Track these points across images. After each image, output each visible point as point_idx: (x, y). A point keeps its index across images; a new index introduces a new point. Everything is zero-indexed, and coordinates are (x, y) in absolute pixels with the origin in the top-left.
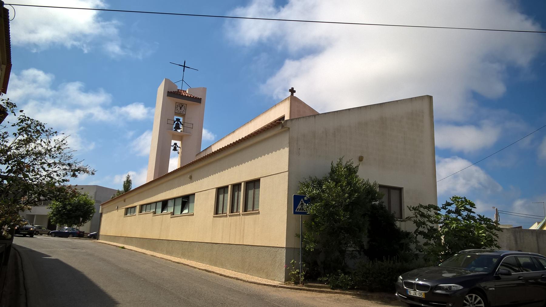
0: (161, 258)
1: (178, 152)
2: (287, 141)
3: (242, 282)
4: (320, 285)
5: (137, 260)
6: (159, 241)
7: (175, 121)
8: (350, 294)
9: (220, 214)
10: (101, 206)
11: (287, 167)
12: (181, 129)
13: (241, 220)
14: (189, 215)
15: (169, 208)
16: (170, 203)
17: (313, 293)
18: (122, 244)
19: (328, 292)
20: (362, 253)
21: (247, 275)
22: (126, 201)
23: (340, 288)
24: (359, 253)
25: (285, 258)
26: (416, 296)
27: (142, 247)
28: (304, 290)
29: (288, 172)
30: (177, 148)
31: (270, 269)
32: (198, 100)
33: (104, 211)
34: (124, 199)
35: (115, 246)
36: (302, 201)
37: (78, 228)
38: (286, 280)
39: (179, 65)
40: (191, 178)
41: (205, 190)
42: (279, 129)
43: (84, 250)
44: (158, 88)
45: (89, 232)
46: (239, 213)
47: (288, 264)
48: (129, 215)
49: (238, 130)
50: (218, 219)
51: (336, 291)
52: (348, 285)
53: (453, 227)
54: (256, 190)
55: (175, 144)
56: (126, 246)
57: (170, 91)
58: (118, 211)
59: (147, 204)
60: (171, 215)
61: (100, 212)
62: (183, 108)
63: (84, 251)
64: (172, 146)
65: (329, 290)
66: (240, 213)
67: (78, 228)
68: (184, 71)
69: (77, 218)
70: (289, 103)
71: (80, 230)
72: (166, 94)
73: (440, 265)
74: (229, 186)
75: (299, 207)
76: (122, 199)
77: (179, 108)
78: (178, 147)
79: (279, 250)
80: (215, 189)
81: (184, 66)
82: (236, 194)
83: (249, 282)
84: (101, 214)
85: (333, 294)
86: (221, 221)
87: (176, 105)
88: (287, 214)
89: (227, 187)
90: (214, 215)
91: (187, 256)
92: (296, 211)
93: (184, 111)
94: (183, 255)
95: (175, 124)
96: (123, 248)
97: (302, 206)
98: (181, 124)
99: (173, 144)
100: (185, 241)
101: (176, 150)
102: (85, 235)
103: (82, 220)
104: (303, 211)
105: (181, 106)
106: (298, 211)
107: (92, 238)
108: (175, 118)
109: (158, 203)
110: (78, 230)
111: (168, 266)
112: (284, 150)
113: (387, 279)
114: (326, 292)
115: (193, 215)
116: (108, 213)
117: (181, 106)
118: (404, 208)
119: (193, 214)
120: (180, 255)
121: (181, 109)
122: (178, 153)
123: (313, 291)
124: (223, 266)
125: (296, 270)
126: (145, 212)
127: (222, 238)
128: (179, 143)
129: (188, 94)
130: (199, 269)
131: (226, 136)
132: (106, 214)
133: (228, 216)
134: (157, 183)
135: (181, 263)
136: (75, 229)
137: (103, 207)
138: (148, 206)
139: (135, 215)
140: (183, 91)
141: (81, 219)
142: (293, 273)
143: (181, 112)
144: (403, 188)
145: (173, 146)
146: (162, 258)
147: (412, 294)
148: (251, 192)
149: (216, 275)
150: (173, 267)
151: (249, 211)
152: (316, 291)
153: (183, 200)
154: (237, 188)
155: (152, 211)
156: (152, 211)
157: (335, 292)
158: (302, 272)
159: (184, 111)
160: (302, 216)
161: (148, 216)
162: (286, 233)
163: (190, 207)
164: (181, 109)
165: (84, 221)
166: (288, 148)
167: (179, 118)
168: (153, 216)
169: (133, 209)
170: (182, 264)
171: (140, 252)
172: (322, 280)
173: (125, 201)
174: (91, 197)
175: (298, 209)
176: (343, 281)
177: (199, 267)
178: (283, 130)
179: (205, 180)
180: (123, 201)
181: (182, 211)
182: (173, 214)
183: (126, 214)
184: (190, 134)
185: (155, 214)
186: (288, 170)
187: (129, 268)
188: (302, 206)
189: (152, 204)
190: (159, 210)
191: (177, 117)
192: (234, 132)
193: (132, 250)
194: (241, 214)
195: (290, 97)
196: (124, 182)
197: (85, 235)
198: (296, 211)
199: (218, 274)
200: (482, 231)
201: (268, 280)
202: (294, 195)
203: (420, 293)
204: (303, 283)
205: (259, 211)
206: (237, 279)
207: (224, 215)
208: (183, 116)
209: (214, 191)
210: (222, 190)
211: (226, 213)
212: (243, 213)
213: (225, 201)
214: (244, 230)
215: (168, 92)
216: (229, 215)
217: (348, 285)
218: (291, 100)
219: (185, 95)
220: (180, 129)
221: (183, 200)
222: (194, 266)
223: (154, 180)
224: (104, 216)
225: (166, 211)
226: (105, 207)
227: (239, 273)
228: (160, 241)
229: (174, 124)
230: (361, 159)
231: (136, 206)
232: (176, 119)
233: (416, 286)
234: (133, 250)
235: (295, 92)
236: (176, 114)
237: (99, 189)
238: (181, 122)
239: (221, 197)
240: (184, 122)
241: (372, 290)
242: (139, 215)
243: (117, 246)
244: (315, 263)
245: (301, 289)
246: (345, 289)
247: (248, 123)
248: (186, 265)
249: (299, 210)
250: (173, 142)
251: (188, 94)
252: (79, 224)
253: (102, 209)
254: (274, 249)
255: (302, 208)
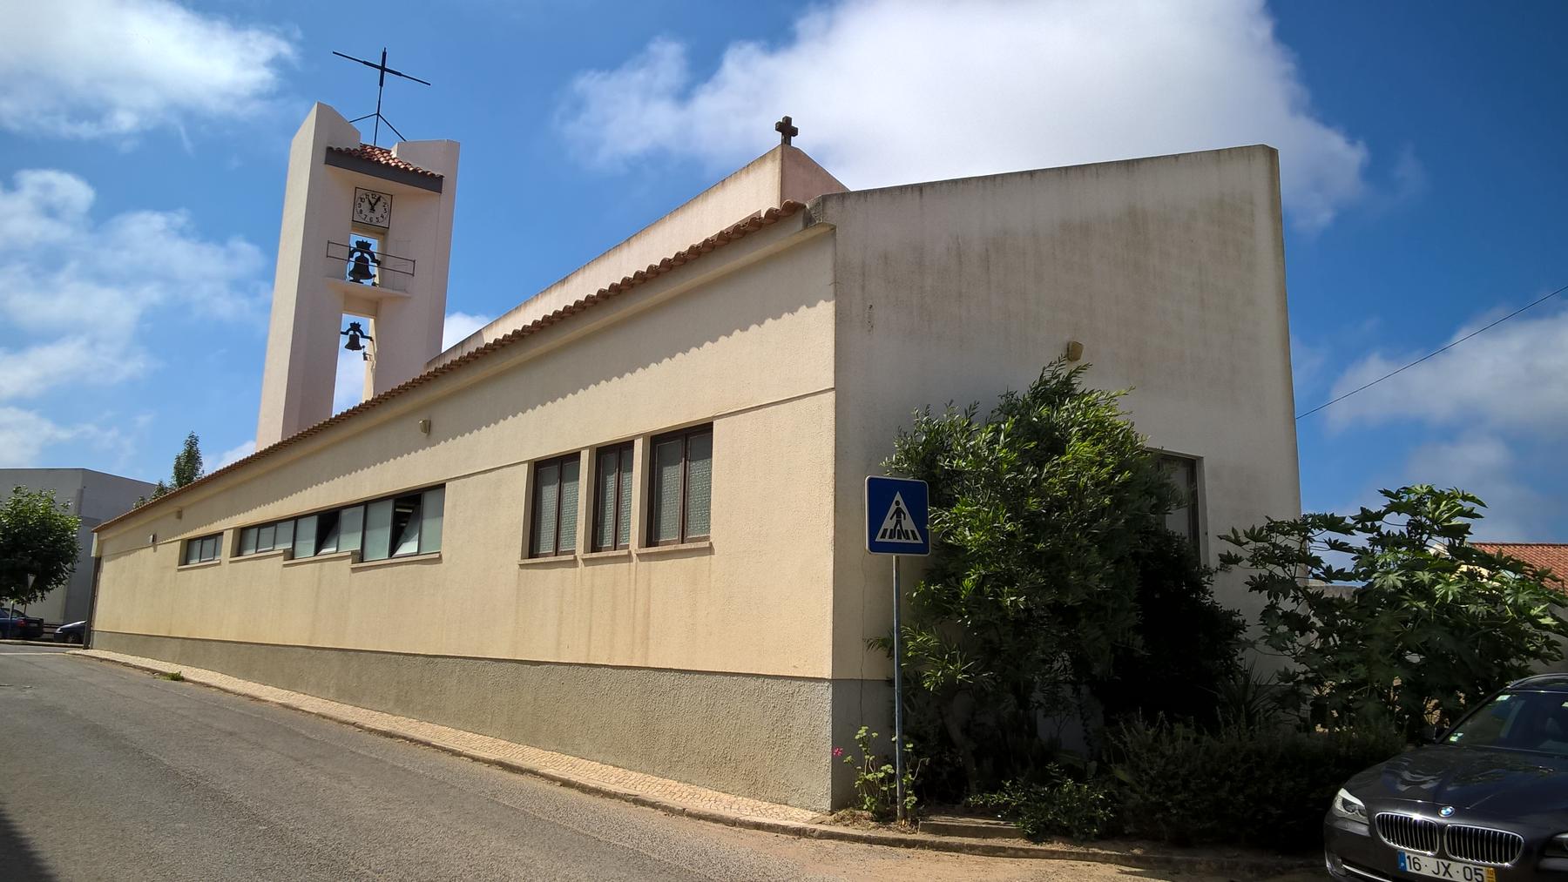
0: (319, 715)
1: (364, 354)
2: (828, 277)
3: (659, 812)
4: (980, 822)
5: (229, 728)
6: (309, 653)
7: (355, 250)
8: (1106, 860)
9: (546, 555)
10: (96, 534)
11: (831, 376)
12: (375, 276)
13: (633, 576)
14: (418, 559)
15: (344, 538)
16: (350, 520)
17: (962, 856)
18: (173, 661)
19: (1021, 853)
20: (1084, 689)
21: (667, 780)
22: (185, 514)
23: (1065, 834)
24: (1074, 690)
25: (828, 718)
26: (1447, 877)
27: (247, 674)
28: (922, 845)
29: (832, 395)
30: (362, 342)
31: (763, 761)
32: (432, 183)
33: (108, 550)
34: (177, 509)
35: (148, 669)
36: (898, 503)
37: (20, 608)
38: (837, 805)
39: (365, 63)
40: (427, 428)
41: (485, 472)
42: (793, 233)
43: (28, 692)
44: (295, 138)
45: (61, 622)
46: (625, 552)
47: (841, 739)
48: (194, 562)
49: (581, 272)
50: (541, 572)
51: (1047, 847)
52: (1092, 821)
53: (1453, 594)
54: (696, 467)
55: (355, 327)
56: (187, 672)
57: (335, 147)
58: (155, 551)
59: (261, 526)
60: (285, 560)
61: (93, 555)
62: (379, 208)
63: (28, 693)
64: (342, 333)
65: (1020, 843)
66: (630, 552)
67: (20, 608)
68: (381, 84)
69: (18, 575)
70: (777, 170)
71: (26, 614)
72: (323, 157)
73: (1453, 739)
74: (582, 452)
75: (888, 523)
76: (170, 509)
77: (366, 206)
78: (363, 337)
79: (802, 689)
80: (526, 465)
81: (383, 69)
82: (611, 481)
83: (690, 815)
84: (98, 562)
85: (1044, 861)
86: (551, 580)
87: (358, 196)
88: (832, 554)
89: (574, 456)
90: (523, 558)
91: (419, 707)
92: (878, 539)
93: (382, 216)
94: (404, 705)
95: (353, 259)
96: (177, 678)
97: (899, 522)
98: (374, 260)
99: (345, 327)
100: (411, 655)
101: (358, 348)
102: (46, 630)
103: (35, 581)
104: (903, 540)
105: (375, 200)
106: (887, 540)
107: (71, 639)
108: (354, 239)
109: (301, 523)
110: (23, 615)
111: (354, 750)
112: (812, 309)
113: (1241, 798)
114: (1012, 852)
115: (439, 560)
116: (122, 558)
117: (373, 201)
118: (1206, 527)
119: (437, 555)
120: (391, 704)
121: (372, 210)
122: (365, 359)
123: (958, 849)
124: (563, 745)
125: (883, 768)
126: (256, 552)
127: (559, 643)
128: (369, 325)
129: (396, 161)
130: (475, 759)
131: (537, 295)
132: (112, 563)
133: (580, 562)
134: (297, 452)
135: (399, 737)
136: (8, 610)
137: (102, 538)
138: (267, 533)
139: (219, 564)
140: (380, 150)
141: (31, 579)
142: (870, 777)
143: (375, 220)
144: (1201, 459)
145: (346, 333)
146: (324, 717)
147: (1426, 872)
148: (672, 475)
149: (542, 784)
150: (373, 756)
151: (668, 543)
152: (971, 849)
153: (397, 510)
154: (612, 458)
155: (280, 548)
156: (280, 548)
157: (1046, 851)
158: (903, 775)
159: (382, 216)
160: (897, 558)
161: (266, 569)
162: (829, 626)
163: (425, 531)
164: (372, 210)
165: (43, 584)
166: (833, 302)
167: (365, 240)
168: (285, 566)
169: (209, 544)
170: (405, 738)
171: (239, 694)
172: (986, 803)
173: (180, 515)
174: (65, 505)
175: (886, 530)
176: (1073, 808)
177: (472, 752)
178: (811, 233)
179: (509, 425)
180: (173, 518)
181: (394, 548)
182: (360, 556)
183: (185, 559)
184: (407, 295)
185: (293, 558)
186: (833, 387)
187: (200, 771)
188: (899, 522)
189: (279, 525)
190: (306, 547)
191: (360, 239)
192: (564, 281)
193: (209, 686)
194: (634, 555)
195: (778, 156)
196: (179, 458)
197: (46, 630)
198: (878, 539)
199: (553, 779)
200: (1542, 607)
201: (759, 803)
202: (870, 480)
203: (1472, 867)
204: (914, 818)
205: (711, 544)
206: (638, 801)
207: (564, 558)
208: (382, 233)
209: (521, 476)
210: (555, 469)
211: (573, 552)
212: (588, 556)
213: (566, 511)
214: (647, 614)
215: (330, 149)
216: (583, 560)
217: (1092, 821)
218: (782, 160)
219: (388, 164)
220: (369, 276)
221: (397, 510)
222: (451, 746)
223: (284, 442)
224: (107, 567)
225: (334, 549)
226: (109, 536)
227: (635, 774)
228: (313, 652)
229: (349, 261)
230: (1072, 352)
231: (221, 534)
232: (357, 242)
233: (1445, 837)
234: (215, 687)
235: (794, 132)
236: (358, 226)
237: (92, 482)
238: (371, 254)
239: (549, 493)
240: (384, 254)
241: (1182, 841)
242: (231, 562)
243: (154, 672)
244: (945, 738)
245: (909, 844)
246: (1082, 837)
247: (618, 247)
248: (421, 742)
249: (890, 538)
250: (347, 320)
251: (396, 161)
252: (23, 595)
253: (101, 544)
254: (778, 686)
255: (898, 528)
